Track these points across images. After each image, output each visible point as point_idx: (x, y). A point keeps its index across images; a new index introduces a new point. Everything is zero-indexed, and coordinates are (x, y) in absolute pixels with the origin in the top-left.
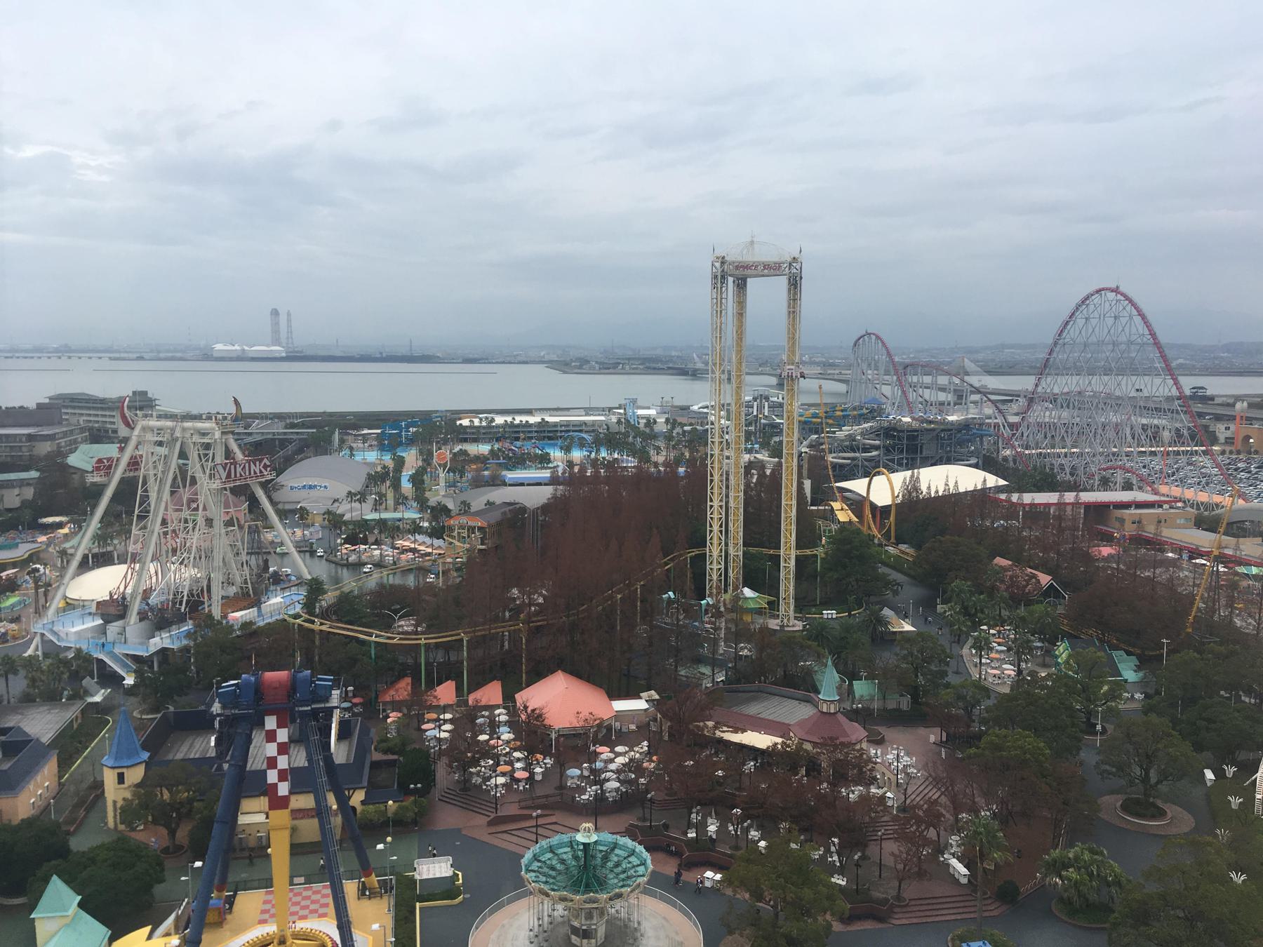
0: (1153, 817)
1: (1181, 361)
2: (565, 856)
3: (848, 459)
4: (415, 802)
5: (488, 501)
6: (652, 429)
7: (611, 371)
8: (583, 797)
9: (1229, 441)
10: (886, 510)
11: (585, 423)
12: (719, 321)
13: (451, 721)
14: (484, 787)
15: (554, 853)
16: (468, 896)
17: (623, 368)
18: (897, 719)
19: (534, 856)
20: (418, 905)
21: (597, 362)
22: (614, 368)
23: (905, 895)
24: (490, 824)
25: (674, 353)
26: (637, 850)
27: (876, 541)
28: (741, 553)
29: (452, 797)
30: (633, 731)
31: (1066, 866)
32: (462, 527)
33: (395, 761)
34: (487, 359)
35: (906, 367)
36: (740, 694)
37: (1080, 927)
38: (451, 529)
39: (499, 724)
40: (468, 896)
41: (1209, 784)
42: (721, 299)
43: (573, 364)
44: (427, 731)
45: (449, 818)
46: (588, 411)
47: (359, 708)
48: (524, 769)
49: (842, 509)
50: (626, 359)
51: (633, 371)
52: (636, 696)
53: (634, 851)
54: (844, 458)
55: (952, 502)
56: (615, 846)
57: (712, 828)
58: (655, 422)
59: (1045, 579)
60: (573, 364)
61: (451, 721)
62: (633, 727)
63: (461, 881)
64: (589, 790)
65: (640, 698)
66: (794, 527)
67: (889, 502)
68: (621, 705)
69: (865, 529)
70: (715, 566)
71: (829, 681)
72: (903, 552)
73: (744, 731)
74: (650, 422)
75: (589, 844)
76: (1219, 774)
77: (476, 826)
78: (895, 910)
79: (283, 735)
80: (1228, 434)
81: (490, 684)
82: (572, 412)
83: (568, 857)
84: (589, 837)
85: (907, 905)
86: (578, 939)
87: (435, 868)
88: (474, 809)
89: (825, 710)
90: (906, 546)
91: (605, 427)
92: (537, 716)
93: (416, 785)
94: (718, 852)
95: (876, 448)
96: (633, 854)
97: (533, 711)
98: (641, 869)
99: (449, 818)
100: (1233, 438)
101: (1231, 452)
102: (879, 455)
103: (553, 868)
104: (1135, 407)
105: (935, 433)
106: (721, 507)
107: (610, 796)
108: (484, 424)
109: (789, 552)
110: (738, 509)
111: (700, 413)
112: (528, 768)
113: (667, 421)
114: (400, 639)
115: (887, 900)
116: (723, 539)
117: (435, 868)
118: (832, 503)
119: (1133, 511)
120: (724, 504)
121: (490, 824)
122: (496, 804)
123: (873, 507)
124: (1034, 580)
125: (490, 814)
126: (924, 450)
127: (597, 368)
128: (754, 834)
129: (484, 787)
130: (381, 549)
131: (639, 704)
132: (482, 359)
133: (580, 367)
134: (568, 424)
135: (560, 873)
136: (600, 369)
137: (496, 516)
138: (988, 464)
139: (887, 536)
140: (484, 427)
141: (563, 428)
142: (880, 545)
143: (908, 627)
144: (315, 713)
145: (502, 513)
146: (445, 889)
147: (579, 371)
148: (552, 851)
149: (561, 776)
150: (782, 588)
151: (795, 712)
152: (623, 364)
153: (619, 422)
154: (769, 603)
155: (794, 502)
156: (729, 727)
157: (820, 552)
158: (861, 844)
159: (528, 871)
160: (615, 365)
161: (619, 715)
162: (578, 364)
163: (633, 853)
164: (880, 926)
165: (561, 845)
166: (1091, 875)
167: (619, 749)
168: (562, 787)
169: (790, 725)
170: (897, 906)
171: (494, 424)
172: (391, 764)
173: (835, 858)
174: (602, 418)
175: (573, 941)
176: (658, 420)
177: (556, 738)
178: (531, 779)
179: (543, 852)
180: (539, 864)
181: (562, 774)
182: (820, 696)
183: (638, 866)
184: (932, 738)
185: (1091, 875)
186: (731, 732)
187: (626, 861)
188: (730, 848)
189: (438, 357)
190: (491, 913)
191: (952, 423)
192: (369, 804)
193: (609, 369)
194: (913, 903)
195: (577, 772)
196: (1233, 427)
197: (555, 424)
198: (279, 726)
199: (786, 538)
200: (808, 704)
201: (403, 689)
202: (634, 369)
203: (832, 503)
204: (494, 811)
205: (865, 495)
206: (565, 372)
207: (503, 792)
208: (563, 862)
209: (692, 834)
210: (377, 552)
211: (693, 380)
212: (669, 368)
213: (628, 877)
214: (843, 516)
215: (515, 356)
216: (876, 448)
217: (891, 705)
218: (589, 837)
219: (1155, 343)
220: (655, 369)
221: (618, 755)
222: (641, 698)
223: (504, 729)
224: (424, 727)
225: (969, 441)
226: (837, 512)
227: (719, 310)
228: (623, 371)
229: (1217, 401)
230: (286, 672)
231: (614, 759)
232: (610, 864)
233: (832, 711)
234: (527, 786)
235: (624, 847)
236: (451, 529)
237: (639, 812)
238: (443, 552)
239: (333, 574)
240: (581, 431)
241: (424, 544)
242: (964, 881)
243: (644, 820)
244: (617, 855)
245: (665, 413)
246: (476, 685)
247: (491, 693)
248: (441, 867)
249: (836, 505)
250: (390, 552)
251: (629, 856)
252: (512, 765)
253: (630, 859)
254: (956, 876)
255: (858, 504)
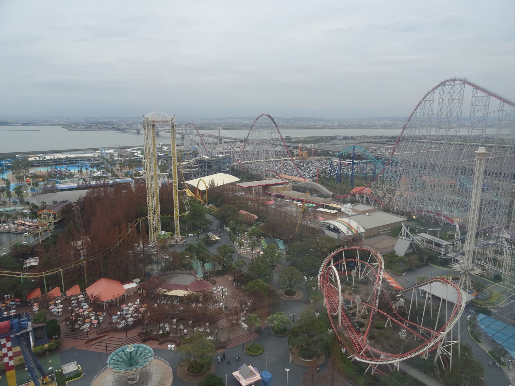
0: (293, 295)
1: (281, 123)
2: (122, 356)
3: (188, 171)
4: (56, 342)
5: (54, 201)
6: (113, 159)
7: (89, 129)
8: (120, 326)
9: (298, 155)
10: (204, 192)
11: (85, 157)
12: (147, 141)
13: (61, 303)
14: (81, 329)
15: (117, 355)
16: (84, 374)
17: (94, 128)
18: (219, 273)
19: (111, 358)
20: (66, 382)
21: (83, 125)
22: (91, 128)
23: (230, 338)
24: (86, 343)
25: (114, 120)
26: (147, 347)
27: (202, 203)
28: (160, 219)
29: (68, 335)
30: (132, 295)
31: (274, 320)
32: (45, 214)
33: (43, 326)
34: (33, 123)
35: (203, 135)
36: (168, 275)
37: (279, 337)
38: (40, 215)
39: (82, 302)
40: (84, 374)
41: (306, 281)
42: (148, 133)
43: (73, 126)
44: (51, 309)
45: (68, 344)
46: (85, 150)
47: (18, 303)
48: (95, 319)
49: (189, 192)
50: (95, 123)
51: (98, 129)
52: (131, 281)
53: (146, 348)
54: (187, 171)
55: (224, 188)
56: (139, 347)
57: (168, 329)
58: (113, 155)
59: (256, 217)
60: (73, 126)
61: (61, 303)
62: (132, 293)
63: (81, 369)
64: (121, 322)
65: (133, 282)
66: (178, 210)
67: (205, 189)
68: (127, 286)
69: (197, 199)
70: (152, 226)
71: (196, 264)
72: (211, 207)
73: (172, 290)
74: (112, 156)
75: (131, 352)
76: (308, 278)
77: (81, 344)
78: (228, 344)
79: (9, 344)
80: (297, 153)
81: (75, 286)
82: (79, 152)
83: (123, 355)
84: (131, 349)
85: (231, 341)
86: (131, 382)
87: (71, 368)
88: (77, 338)
89: (199, 280)
90: (211, 205)
91: (94, 158)
92: (97, 299)
93: (55, 336)
94: (172, 337)
95: (197, 167)
96: (145, 349)
97: (95, 296)
98: (150, 354)
99: (68, 344)
100: (298, 154)
101: (298, 159)
102: (198, 170)
103: (118, 361)
104: (271, 144)
105: (216, 161)
106: (152, 205)
107: (131, 323)
108: (41, 159)
109: (177, 215)
110: (157, 204)
111: (131, 152)
112: (97, 318)
113: (118, 155)
114: (34, 275)
115: (225, 341)
116: (154, 216)
117: (71, 368)
118: (185, 189)
119: (276, 186)
120: (153, 204)
121: (86, 343)
122: (88, 335)
123: (200, 191)
124: (253, 218)
125: (85, 339)
126: (213, 167)
127: (84, 128)
128: (182, 327)
129: (81, 329)
130: (8, 225)
131: (133, 285)
132: (31, 123)
133: (76, 127)
134: (77, 158)
135: (121, 362)
136: (85, 128)
137: (59, 208)
138: (233, 172)
139: (205, 201)
140: (41, 161)
141: (76, 159)
142: (203, 205)
143: (217, 238)
144: (22, 335)
145: (62, 207)
146: (77, 374)
147: (76, 129)
148: (117, 355)
149: (110, 319)
150: (175, 230)
151: (188, 279)
152: (94, 126)
153: (99, 156)
154: (171, 235)
155: (178, 201)
156: (167, 289)
157: (186, 214)
158: (215, 323)
159: (110, 364)
160: (91, 127)
161: (128, 290)
162: (75, 126)
163: (145, 349)
164: (225, 350)
165: (120, 352)
166: (281, 321)
167: (129, 304)
168: (111, 323)
169: (188, 286)
170: (229, 342)
171: (45, 159)
172: (42, 327)
173: (208, 330)
174: (92, 155)
175: (129, 383)
176: (114, 155)
177: (105, 305)
178: (99, 323)
179: (114, 356)
180: (113, 361)
181: (111, 319)
182: (197, 276)
183: (148, 353)
184: (230, 279)
185: (281, 321)
186: (168, 291)
187: (144, 352)
188: (174, 334)
189: (10, 123)
190: (95, 379)
191: (221, 157)
192: (37, 346)
193: (88, 128)
194: (233, 340)
195: (116, 317)
196: (298, 151)
197: (72, 158)
198: (7, 341)
199: (176, 213)
200: (191, 275)
201: (37, 293)
202: (99, 128)
203: (185, 189)
204: (87, 337)
205: (197, 187)
206: (70, 130)
207: (89, 329)
208: (121, 357)
209: (161, 332)
210: (7, 227)
211: (123, 133)
212: (113, 128)
213: (146, 358)
214: (189, 195)
215: (46, 122)
216: (197, 167)
217: (216, 269)
218: (131, 349)
219: (277, 126)
220: (107, 128)
221: (129, 307)
222: (133, 282)
223: (84, 304)
224: (50, 308)
225: (226, 163)
226: (187, 193)
227: (147, 137)
228: (94, 129)
229: (293, 140)
230: (7, 321)
231: (129, 308)
232: (138, 355)
233: (201, 280)
234: (98, 325)
235: (142, 347)
236: (40, 215)
237: (141, 327)
238: (37, 224)
239: (38, 297)
240: (83, 160)
241: (28, 222)
242: (246, 329)
243: (143, 329)
244: (140, 351)
245: (117, 151)
246: (68, 287)
247: (75, 290)
248: (72, 366)
249: (187, 190)
250: (13, 226)
251: (144, 350)
252: (90, 318)
253: (145, 351)
254: (244, 328)
255: (194, 189)
